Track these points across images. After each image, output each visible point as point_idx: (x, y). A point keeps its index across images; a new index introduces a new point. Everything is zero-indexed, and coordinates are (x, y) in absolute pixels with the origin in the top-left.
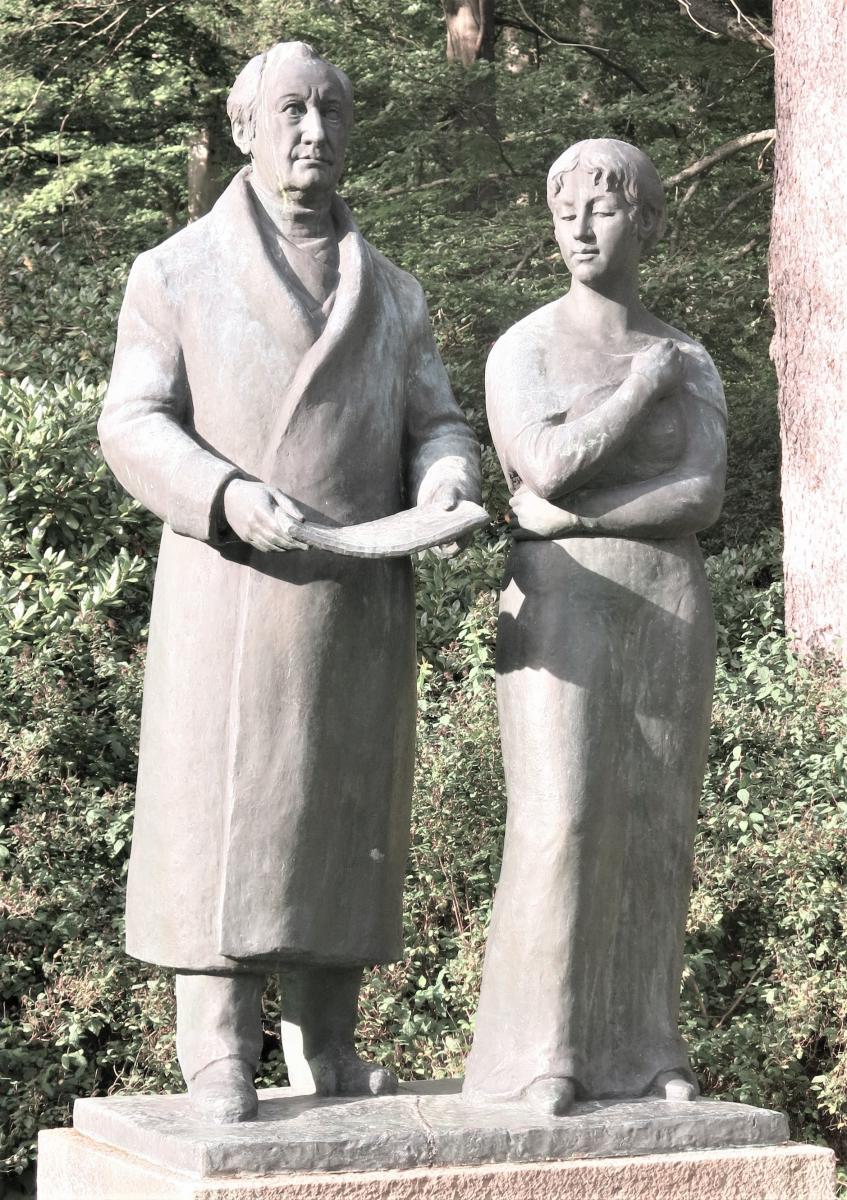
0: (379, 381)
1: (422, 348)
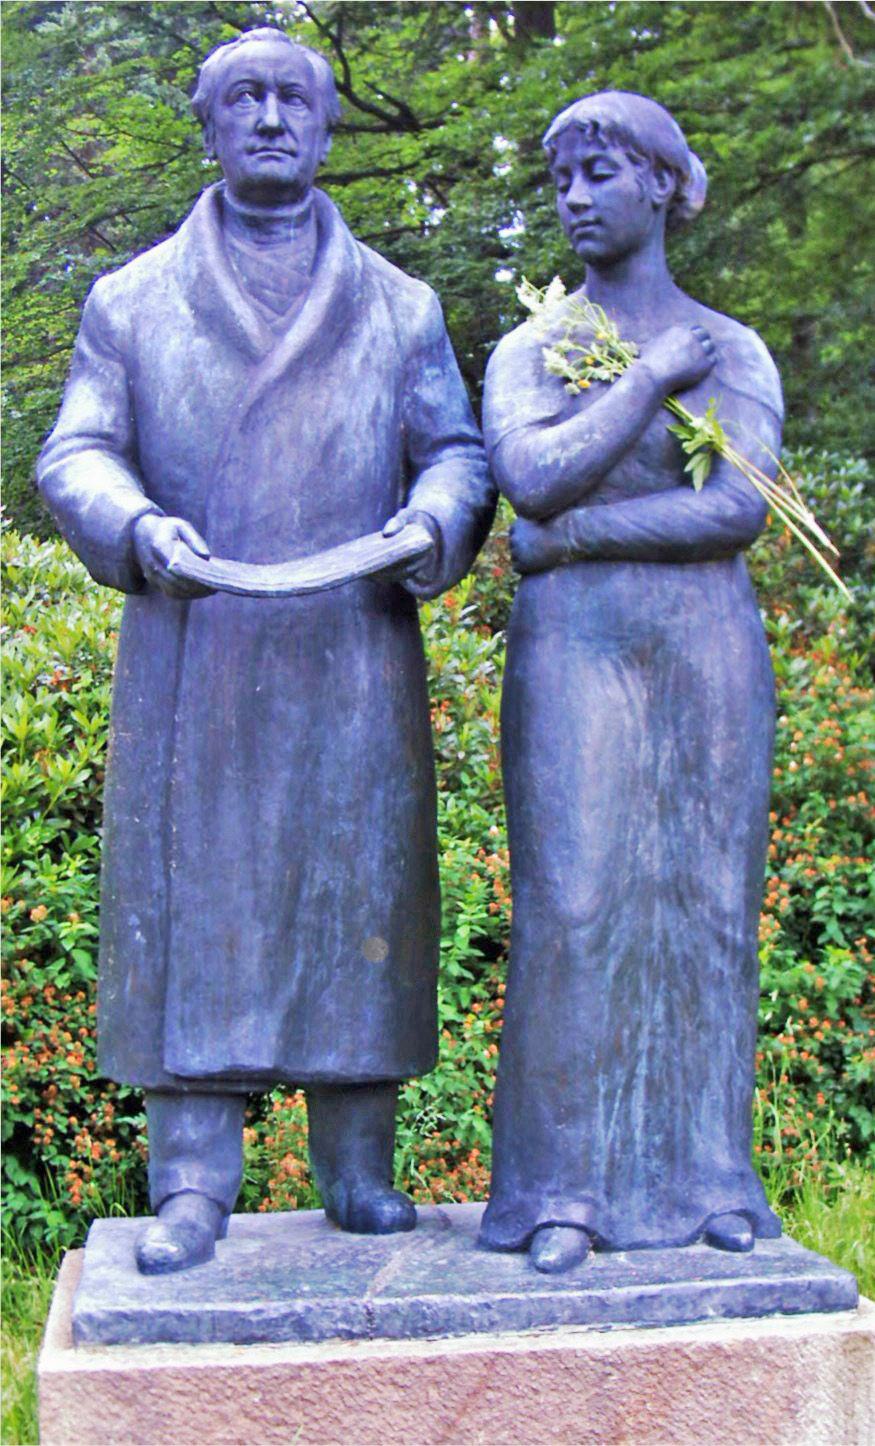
0: (353, 397)
1: (425, 363)
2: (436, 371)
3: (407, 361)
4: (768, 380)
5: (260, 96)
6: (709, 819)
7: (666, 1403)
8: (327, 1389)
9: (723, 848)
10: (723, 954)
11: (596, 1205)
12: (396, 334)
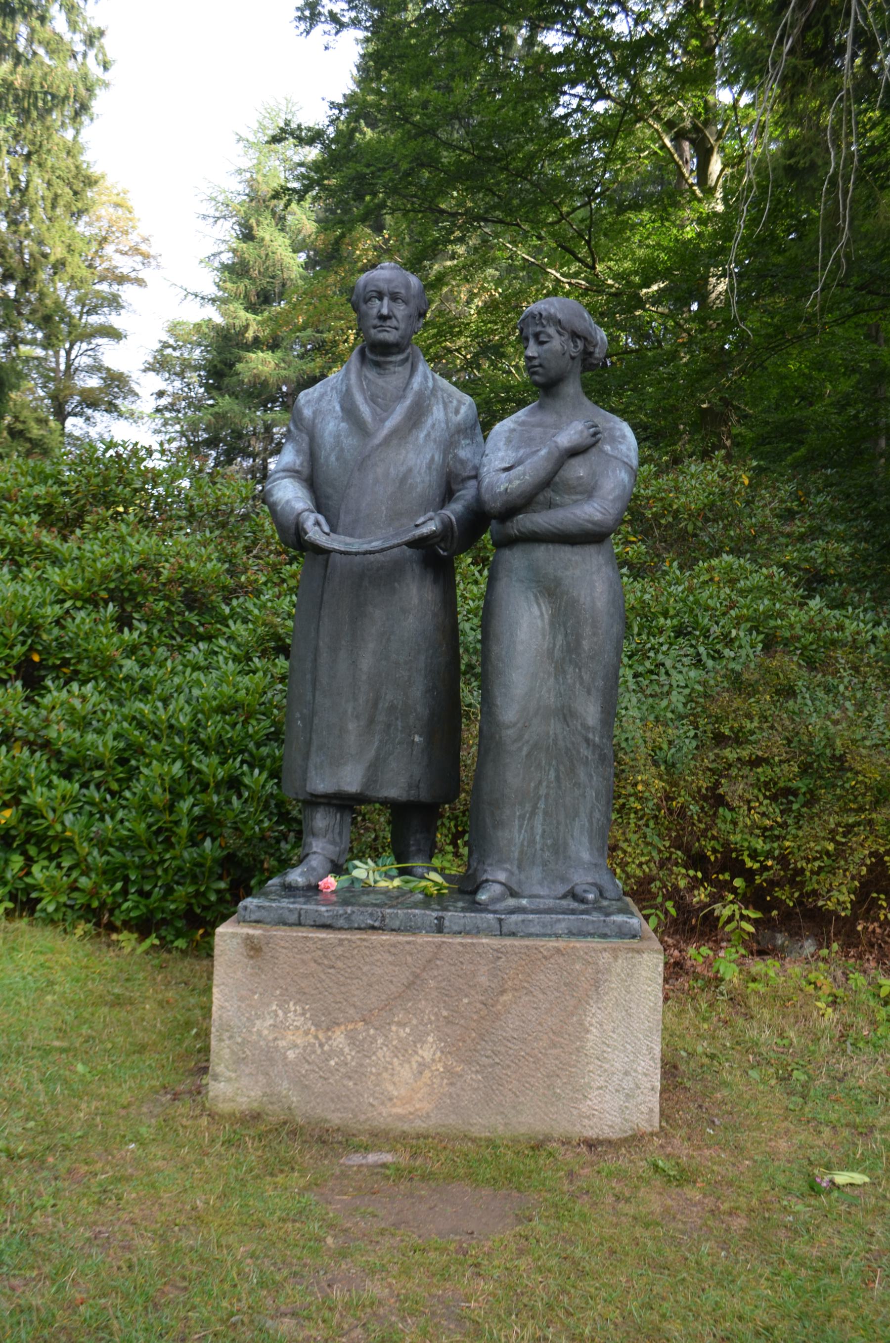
2: (468, 441)
3: (452, 436)
4: (629, 449)
5: (381, 299)
6: (581, 677)
7: (529, 975)
8: (356, 952)
9: (589, 692)
10: (588, 748)
11: (512, 873)
12: (447, 423)
